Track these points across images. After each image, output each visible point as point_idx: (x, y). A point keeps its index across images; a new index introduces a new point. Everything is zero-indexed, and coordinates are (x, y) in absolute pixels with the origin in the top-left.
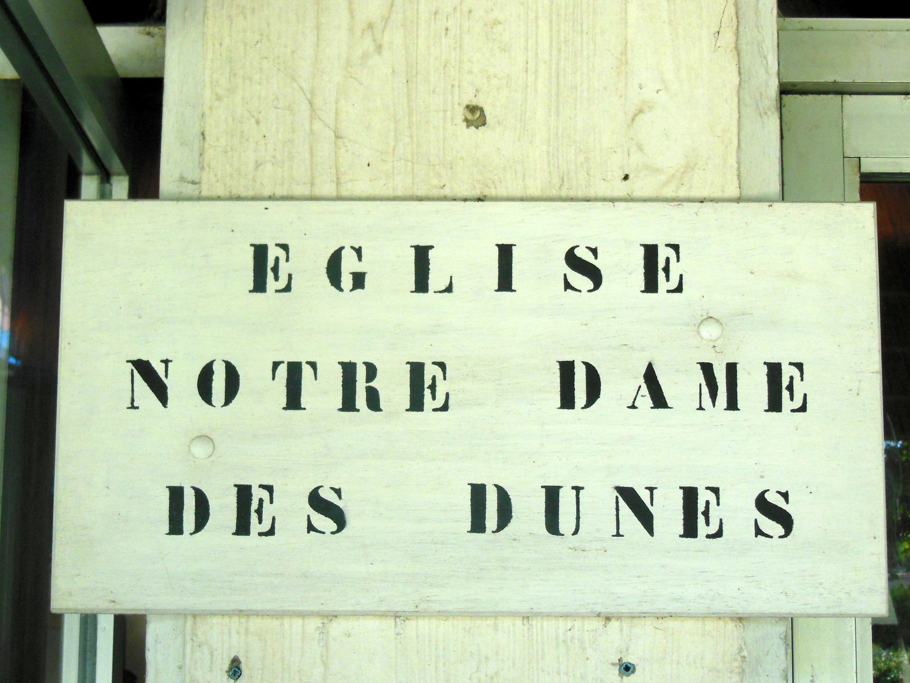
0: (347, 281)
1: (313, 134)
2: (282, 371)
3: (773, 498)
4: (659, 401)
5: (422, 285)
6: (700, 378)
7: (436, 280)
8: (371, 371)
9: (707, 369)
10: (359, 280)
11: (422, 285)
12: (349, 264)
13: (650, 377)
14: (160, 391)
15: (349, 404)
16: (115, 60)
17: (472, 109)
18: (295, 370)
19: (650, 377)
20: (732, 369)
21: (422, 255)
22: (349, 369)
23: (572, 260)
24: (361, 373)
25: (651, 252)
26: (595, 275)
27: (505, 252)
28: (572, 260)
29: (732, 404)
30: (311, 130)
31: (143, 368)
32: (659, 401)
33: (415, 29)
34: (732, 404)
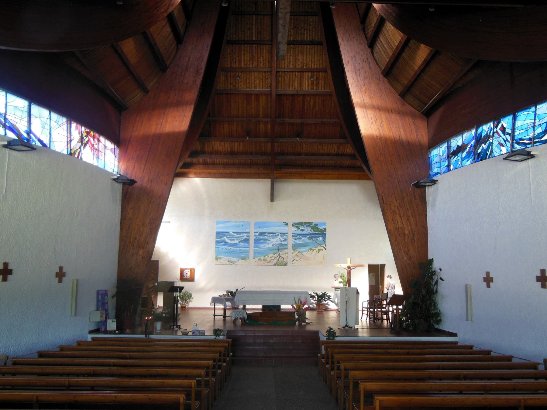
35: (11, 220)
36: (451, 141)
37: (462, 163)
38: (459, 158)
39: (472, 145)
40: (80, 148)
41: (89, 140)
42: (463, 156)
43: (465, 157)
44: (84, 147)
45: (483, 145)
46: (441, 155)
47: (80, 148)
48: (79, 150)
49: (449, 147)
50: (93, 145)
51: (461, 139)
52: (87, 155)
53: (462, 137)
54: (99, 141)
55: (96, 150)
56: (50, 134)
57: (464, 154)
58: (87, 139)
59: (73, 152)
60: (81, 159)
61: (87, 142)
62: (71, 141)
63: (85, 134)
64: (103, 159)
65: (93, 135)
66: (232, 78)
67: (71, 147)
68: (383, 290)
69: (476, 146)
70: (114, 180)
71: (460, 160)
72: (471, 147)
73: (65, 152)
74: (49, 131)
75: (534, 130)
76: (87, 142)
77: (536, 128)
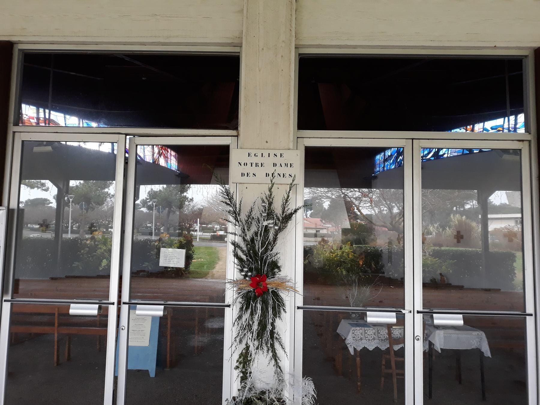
0: (256, 156)
1: (44, 222)
2: (251, 163)
3: (290, 174)
4: (281, 166)
5: (262, 157)
6: (285, 164)
7: (263, 156)
8: (258, 164)
9: (285, 164)
10: (257, 156)
11: (262, 157)
12: (256, 155)
13: (281, 164)
14: (241, 165)
15: (256, 166)
16: (338, 180)
17: (267, 141)
18: (252, 163)
19: (281, 164)
20: (287, 164)
21: (262, 154)
22: (256, 163)
23: (275, 155)
24: (257, 164)
25: (281, 154)
26: (276, 156)
27: (269, 154)
28: (275, 155)
29: (287, 167)
30: (226, 283)
31: (239, 163)
32: (281, 166)
33: (364, 39)
34: (287, 167)
35: (374, 390)
36: (386, 152)
37: (390, 166)
38: (389, 163)
39: (395, 156)
40: (158, 158)
41: (163, 151)
42: (391, 162)
43: (391, 163)
44: (160, 157)
45: (400, 157)
46: (381, 160)
47: (158, 158)
48: (158, 159)
49: (384, 155)
50: (165, 155)
51: (390, 151)
52: (162, 162)
53: (391, 150)
54: (168, 152)
55: (166, 158)
56: (144, 151)
57: (391, 161)
58: (161, 152)
59: (155, 160)
60: (159, 164)
61: (162, 154)
62: (154, 154)
63: (160, 149)
64: (170, 162)
65: (164, 148)
66: (125, 308)
67: (154, 158)
68: (124, 230)
69: (397, 158)
70: (177, 175)
71: (389, 165)
72: (395, 157)
73: (151, 162)
74: (143, 150)
75: (424, 152)
76: (162, 154)
77: (425, 150)
